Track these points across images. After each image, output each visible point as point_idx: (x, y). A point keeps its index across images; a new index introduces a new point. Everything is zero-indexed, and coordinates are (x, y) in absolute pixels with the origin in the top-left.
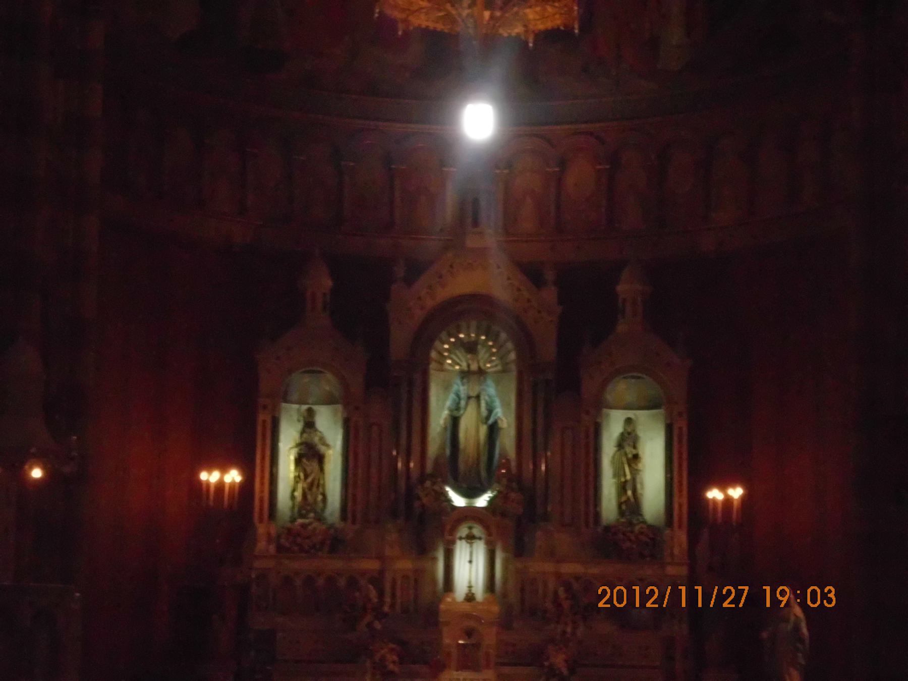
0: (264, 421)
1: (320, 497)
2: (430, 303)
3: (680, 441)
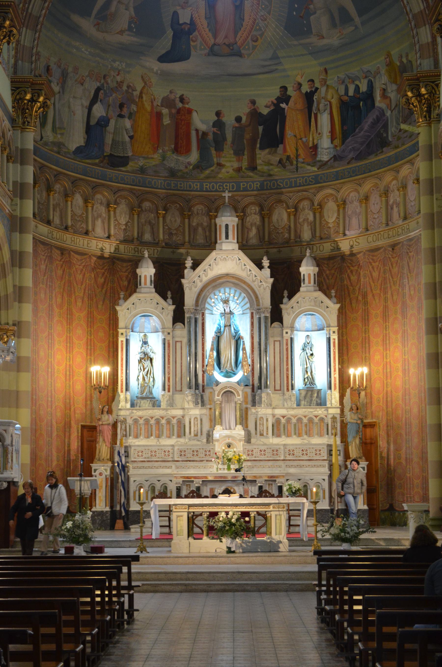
1: (151, 380)
3: (334, 346)
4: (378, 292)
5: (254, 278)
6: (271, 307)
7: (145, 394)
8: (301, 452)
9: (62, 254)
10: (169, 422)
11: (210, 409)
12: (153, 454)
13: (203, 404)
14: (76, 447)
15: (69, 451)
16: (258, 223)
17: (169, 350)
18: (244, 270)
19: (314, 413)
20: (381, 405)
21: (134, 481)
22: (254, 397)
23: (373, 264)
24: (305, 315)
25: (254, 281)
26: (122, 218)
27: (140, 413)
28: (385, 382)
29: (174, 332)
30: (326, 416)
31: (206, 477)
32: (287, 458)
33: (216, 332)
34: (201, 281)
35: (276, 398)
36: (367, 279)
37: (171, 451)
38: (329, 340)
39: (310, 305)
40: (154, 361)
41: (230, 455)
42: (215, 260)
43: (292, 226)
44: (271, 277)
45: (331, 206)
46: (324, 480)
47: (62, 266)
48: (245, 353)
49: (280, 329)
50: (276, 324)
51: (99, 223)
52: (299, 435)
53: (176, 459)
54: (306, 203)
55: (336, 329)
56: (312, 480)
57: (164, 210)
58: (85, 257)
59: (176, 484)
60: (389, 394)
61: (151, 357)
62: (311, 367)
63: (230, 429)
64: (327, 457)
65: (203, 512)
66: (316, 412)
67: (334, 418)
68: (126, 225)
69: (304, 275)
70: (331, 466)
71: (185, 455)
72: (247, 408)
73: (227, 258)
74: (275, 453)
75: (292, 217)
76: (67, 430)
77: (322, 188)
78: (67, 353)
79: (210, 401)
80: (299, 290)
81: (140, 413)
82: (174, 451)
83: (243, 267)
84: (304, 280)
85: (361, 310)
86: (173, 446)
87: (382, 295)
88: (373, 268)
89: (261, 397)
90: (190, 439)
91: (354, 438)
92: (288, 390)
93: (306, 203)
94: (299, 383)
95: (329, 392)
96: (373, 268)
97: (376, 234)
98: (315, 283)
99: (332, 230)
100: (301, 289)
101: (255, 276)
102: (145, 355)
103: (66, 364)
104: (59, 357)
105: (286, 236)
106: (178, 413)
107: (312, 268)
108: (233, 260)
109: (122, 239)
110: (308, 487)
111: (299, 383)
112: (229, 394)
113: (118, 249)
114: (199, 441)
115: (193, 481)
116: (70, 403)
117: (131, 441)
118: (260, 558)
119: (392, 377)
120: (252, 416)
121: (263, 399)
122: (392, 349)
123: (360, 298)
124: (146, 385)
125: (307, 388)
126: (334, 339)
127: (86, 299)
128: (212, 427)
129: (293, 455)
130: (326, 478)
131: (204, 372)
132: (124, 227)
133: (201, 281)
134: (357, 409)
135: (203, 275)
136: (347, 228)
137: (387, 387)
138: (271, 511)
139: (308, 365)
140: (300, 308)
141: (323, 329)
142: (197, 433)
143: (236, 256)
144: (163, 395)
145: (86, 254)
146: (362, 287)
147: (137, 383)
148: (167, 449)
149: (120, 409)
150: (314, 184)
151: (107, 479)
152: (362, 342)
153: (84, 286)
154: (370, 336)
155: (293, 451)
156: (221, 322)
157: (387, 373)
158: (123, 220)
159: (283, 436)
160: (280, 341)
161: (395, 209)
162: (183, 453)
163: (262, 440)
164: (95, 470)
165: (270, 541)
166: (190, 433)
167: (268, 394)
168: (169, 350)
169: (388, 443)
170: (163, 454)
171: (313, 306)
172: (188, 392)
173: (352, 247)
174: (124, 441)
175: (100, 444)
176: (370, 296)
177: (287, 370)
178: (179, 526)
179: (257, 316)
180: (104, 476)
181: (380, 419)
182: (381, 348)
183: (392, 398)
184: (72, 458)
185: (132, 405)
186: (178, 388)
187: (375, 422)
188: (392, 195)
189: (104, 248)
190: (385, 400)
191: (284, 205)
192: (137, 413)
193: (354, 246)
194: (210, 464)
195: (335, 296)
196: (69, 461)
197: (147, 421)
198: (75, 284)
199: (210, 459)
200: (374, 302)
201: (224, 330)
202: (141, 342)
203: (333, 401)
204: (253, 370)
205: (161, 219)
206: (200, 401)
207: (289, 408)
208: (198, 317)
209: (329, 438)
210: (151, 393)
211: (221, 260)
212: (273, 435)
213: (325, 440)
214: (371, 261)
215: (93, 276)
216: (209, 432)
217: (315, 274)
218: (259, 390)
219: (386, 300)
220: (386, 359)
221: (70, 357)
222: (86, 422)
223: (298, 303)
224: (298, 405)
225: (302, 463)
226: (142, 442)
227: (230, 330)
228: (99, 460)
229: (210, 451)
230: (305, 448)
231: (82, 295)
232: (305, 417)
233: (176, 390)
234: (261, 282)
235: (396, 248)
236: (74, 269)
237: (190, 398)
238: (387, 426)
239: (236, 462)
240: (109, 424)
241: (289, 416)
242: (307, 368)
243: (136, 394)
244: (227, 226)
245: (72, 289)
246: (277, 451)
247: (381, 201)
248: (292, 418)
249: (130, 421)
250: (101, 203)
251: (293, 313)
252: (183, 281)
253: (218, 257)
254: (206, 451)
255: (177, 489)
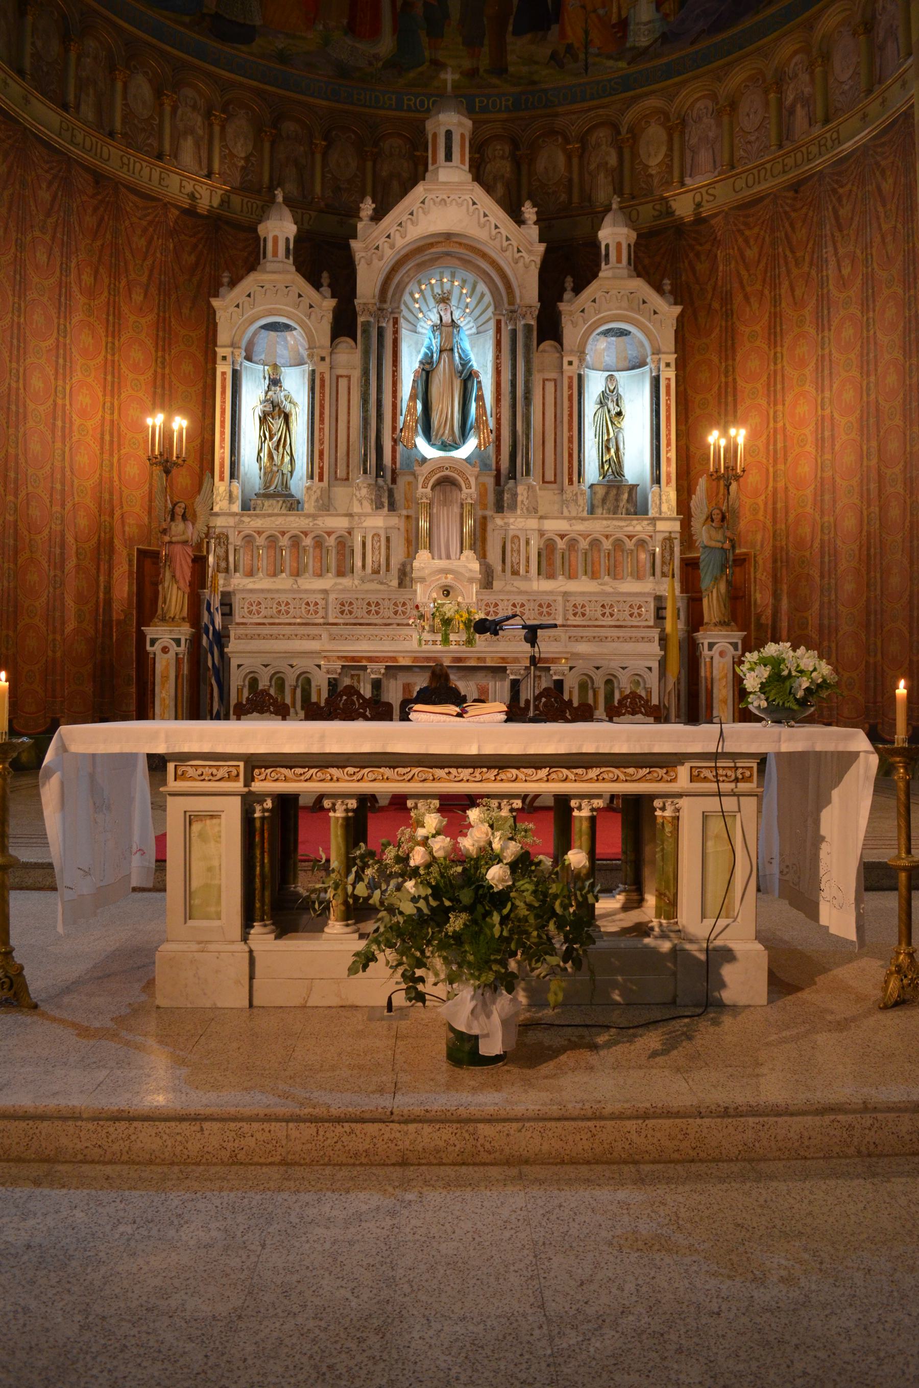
0: (224, 374)
1: (287, 459)
2: (400, 242)
3: (668, 393)
4: (758, 286)
5: (505, 244)
6: (539, 305)
7: (272, 488)
8: (599, 609)
9: (97, 183)
10: (319, 543)
11: (408, 517)
12: (283, 608)
13: (392, 507)
14: (125, 595)
15: (108, 602)
16: (508, 175)
17: (322, 393)
18: (485, 225)
19: (626, 529)
20: (762, 518)
21: (239, 666)
22: (499, 495)
23: (747, 233)
24: (606, 333)
25: (504, 250)
26: (239, 144)
27: (258, 523)
28: (771, 470)
29: (334, 356)
30: (651, 537)
31: (394, 659)
32: (569, 623)
33: (421, 362)
34: (392, 247)
35: (547, 498)
36: (733, 265)
37: (322, 603)
38: (656, 383)
39: (620, 308)
40: (293, 419)
41: (449, 609)
42: (423, 202)
43: (575, 176)
44: (541, 241)
45: (655, 132)
46: (650, 669)
47: (96, 209)
48: (481, 407)
49: (558, 355)
50: (547, 345)
51: (188, 144)
52: (594, 576)
53: (331, 620)
54: (603, 134)
55: (672, 358)
56: (623, 668)
57: (325, 140)
58: (154, 204)
59: (328, 672)
60: (781, 495)
61: (287, 410)
62: (616, 439)
63: (448, 557)
64: (655, 623)
65: (321, 797)
66: (630, 528)
67: (668, 540)
68: (247, 159)
69: (607, 246)
70: (663, 640)
71: (351, 612)
72: (484, 518)
73: (448, 201)
74: (545, 610)
75: (575, 161)
76: (105, 557)
77: (635, 99)
78: (104, 395)
79: (406, 499)
80: (595, 276)
81: (258, 523)
82: (327, 604)
83: (483, 220)
84: (607, 255)
85: (718, 329)
86: (325, 592)
87: (766, 292)
88: (746, 241)
89: (515, 495)
90: (363, 581)
91: (716, 580)
92: (571, 481)
93: (603, 134)
94: (592, 472)
95: (655, 488)
96: (746, 241)
97: (755, 171)
98: (629, 263)
99: (656, 181)
100: (601, 274)
101: (508, 239)
102: (274, 407)
103: (103, 417)
104: (83, 399)
105: (562, 199)
106: (339, 523)
107: (625, 230)
108: (462, 205)
109: (237, 184)
110: (616, 685)
111: (592, 472)
112: (448, 488)
113: (228, 202)
114: (382, 583)
115: (364, 668)
116: (111, 500)
117: (238, 581)
118: (667, 1123)
119: (789, 459)
120: (496, 532)
121: (520, 498)
122: (789, 399)
123: (716, 305)
124: (275, 469)
125: (608, 481)
126: (669, 379)
127: (153, 290)
128: (411, 555)
129: (584, 615)
130: (655, 665)
131: (395, 441)
132: (242, 163)
133: (392, 247)
134: (723, 518)
135: (398, 234)
136: (689, 172)
137: (775, 480)
138: (680, 796)
139: (612, 435)
140: (599, 312)
141: (642, 364)
142: (379, 566)
143: (467, 197)
144: (308, 488)
145: (158, 200)
146: (720, 283)
147: (257, 465)
148: (312, 598)
149: (216, 514)
150: (621, 92)
151: (178, 661)
152: (719, 394)
153: (149, 262)
154: (738, 379)
155: (583, 606)
156: (434, 341)
157: (775, 452)
158: (241, 149)
159: (561, 578)
160: (555, 380)
161: (800, 112)
162: (346, 608)
163: (516, 584)
164: (153, 642)
165: (674, 950)
166: (364, 566)
167: (530, 488)
168: (322, 393)
169: (776, 595)
170: (303, 610)
171: (627, 310)
172: (359, 479)
173: (699, 205)
174: (221, 582)
175: (166, 585)
176: (738, 299)
177: (570, 440)
178: (197, 867)
179: (509, 328)
180: (172, 654)
181: (758, 548)
182: (763, 402)
183: (786, 501)
184: (115, 616)
185: (245, 507)
186: (341, 473)
187: (746, 554)
188: (792, 86)
189: (197, 196)
190: (770, 506)
191: (560, 140)
192: (253, 523)
193: (704, 203)
194: (405, 631)
195: (671, 292)
196: (108, 624)
197: (272, 540)
198: (129, 255)
199: (405, 622)
200: (748, 309)
201: (440, 358)
202: (267, 381)
203: (664, 508)
204: (498, 438)
205: (318, 157)
206: (385, 501)
207: (575, 518)
208: (384, 325)
209: (657, 583)
210: (286, 486)
211: (435, 203)
212: (539, 574)
213: (647, 586)
214: (742, 227)
215: (171, 246)
216: (404, 565)
217: (629, 245)
218: (512, 481)
219: (776, 301)
220: (775, 421)
221: (112, 404)
222: (150, 545)
223: (594, 301)
224: (592, 511)
225: (603, 632)
226: (261, 582)
227: (452, 359)
228: (163, 619)
229: (404, 604)
230: (608, 601)
231: (144, 279)
232: (607, 537)
233: (336, 479)
234: (519, 251)
235: (802, 189)
236: (127, 223)
237: (364, 492)
238: (775, 561)
239: (462, 626)
240: (185, 542)
241: (573, 535)
242: (608, 440)
243: (257, 491)
244: (449, 134)
245: (122, 264)
246: (549, 606)
247: (767, 104)
248: (580, 539)
249: (235, 539)
250: (194, 107)
251: (585, 323)
252: (354, 244)
253: (430, 197)
254: (395, 604)
255: (329, 683)
